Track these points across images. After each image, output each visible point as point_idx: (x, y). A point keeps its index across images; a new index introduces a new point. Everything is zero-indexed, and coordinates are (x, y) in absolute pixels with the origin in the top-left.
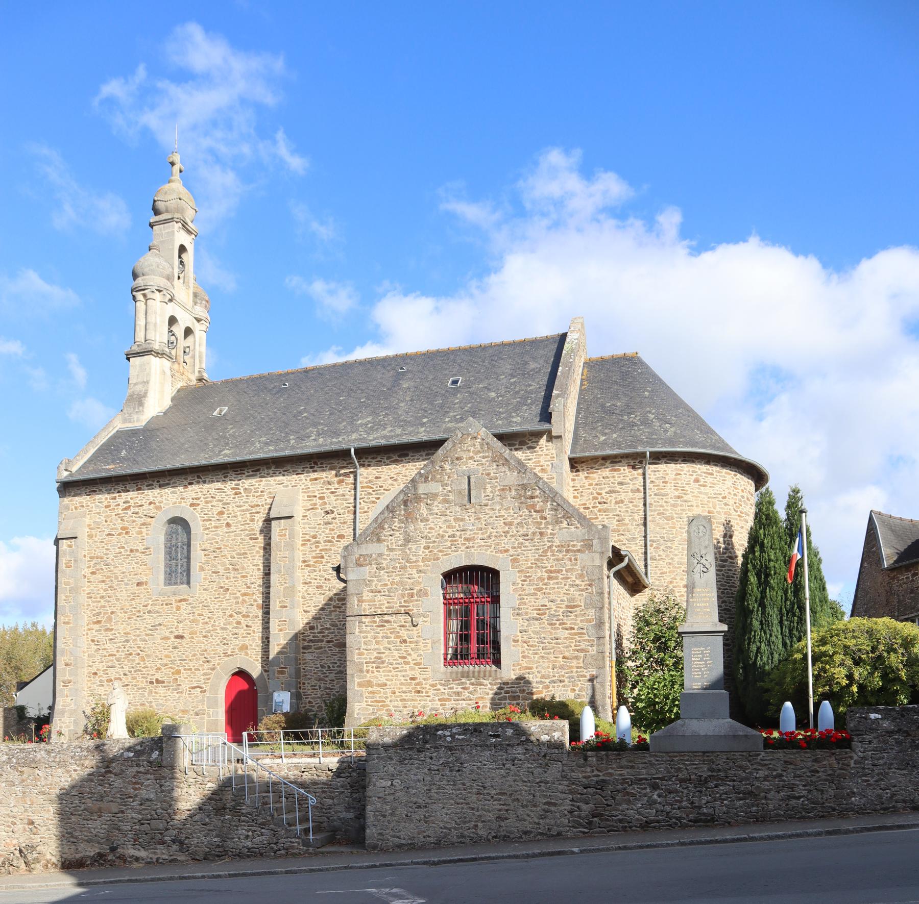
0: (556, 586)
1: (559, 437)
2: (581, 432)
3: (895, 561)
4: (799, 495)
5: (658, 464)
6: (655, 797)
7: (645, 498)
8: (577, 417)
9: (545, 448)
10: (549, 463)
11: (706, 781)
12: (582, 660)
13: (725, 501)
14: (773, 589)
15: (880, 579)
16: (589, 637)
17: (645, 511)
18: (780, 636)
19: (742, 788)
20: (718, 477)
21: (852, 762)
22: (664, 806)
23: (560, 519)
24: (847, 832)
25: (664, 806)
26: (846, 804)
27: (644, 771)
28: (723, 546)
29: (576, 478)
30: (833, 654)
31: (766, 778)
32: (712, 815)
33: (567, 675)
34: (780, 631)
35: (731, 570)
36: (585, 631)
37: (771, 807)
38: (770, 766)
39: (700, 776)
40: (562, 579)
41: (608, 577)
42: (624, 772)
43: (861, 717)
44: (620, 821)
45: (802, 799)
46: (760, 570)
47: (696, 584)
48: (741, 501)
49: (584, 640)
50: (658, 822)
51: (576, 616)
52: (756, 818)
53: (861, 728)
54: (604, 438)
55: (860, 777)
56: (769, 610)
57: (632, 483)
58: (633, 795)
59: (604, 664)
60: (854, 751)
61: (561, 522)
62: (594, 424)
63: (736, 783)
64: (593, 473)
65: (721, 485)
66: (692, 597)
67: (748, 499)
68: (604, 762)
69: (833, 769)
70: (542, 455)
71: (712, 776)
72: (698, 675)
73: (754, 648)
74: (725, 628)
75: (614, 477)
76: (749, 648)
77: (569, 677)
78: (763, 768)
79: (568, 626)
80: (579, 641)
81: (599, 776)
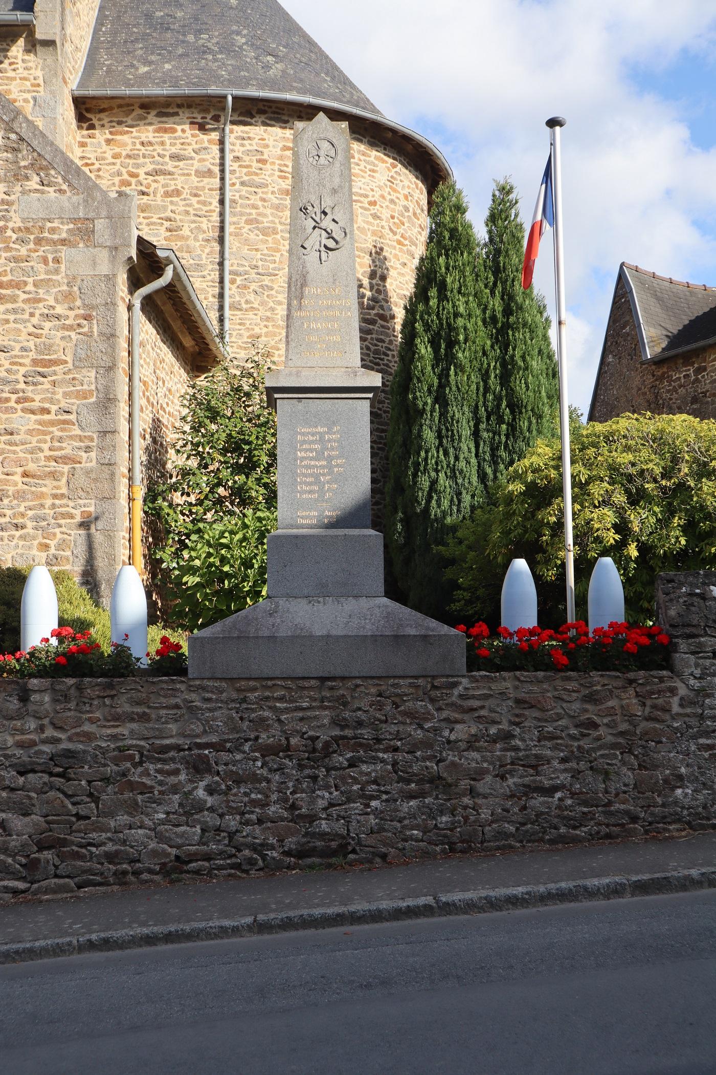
0: (12, 317)
1: (50, 43)
2: (103, 57)
3: (663, 349)
4: (511, 197)
5: (250, 124)
6: (201, 793)
7: (222, 189)
8: (96, 31)
9: (20, 65)
10: (28, 96)
11: (327, 750)
12: (64, 480)
13: (374, 209)
14: (463, 371)
15: (637, 382)
16: (82, 429)
17: (222, 214)
18: (474, 461)
19: (415, 769)
20: (363, 164)
21: (675, 701)
22: (221, 816)
23: (23, 172)
24: (687, 884)
25: (221, 816)
26: (664, 805)
27: (173, 727)
28: (368, 294)
29: (88, 140)
30: (587, 483)
31: (472, 743)
32: (343, 837)
33: (30, 513)
34: (473, 450)
35: (383, 341)
36: (72, 417)
37: (485, 814)
38: (483, 713)
39: (314, 739)
40: (25, 301)
41: (130, 308)
42: (124, 730)
43: (692, 595)
44: (111, 857)
45: (558, 795)
46: (438, 334)
47: (309, 277)
48: (403, 215)
49: (71, 437)
50: (208, 857)
51: (54, 383)
52: (452, 844)
53: (695, 618)
54: (146, 69)
55: (695, 737)
56: (453, 409)
57: (197, 157)
58: (145, 789)
59: (113, 489)
60: (679, 675)
61: (27, 178)
62: (129, 45)
63: (399, 756)
64: (121, 133)
65: (367, 179)
66: (300, 308)
67: (415, 214)
68: (72, 705)
69: (630, 718)
70: (14, 79)
71: (343, 738)
72: (310, 492)
73: (424, 482)
74: (375, 379)
75: (162, 143)
76: (415, 483)
77: (36, 519)
78: (466, 717)
79: (36, 405)
80: (60, 440)
81: (58, 741)
